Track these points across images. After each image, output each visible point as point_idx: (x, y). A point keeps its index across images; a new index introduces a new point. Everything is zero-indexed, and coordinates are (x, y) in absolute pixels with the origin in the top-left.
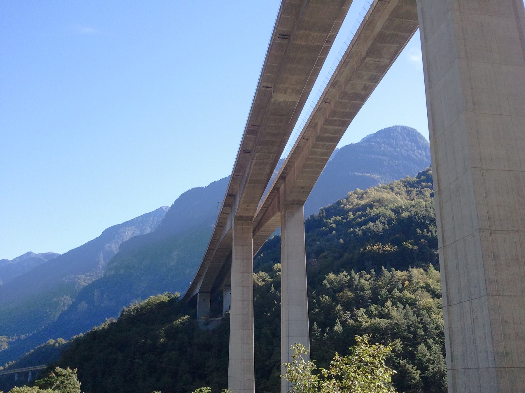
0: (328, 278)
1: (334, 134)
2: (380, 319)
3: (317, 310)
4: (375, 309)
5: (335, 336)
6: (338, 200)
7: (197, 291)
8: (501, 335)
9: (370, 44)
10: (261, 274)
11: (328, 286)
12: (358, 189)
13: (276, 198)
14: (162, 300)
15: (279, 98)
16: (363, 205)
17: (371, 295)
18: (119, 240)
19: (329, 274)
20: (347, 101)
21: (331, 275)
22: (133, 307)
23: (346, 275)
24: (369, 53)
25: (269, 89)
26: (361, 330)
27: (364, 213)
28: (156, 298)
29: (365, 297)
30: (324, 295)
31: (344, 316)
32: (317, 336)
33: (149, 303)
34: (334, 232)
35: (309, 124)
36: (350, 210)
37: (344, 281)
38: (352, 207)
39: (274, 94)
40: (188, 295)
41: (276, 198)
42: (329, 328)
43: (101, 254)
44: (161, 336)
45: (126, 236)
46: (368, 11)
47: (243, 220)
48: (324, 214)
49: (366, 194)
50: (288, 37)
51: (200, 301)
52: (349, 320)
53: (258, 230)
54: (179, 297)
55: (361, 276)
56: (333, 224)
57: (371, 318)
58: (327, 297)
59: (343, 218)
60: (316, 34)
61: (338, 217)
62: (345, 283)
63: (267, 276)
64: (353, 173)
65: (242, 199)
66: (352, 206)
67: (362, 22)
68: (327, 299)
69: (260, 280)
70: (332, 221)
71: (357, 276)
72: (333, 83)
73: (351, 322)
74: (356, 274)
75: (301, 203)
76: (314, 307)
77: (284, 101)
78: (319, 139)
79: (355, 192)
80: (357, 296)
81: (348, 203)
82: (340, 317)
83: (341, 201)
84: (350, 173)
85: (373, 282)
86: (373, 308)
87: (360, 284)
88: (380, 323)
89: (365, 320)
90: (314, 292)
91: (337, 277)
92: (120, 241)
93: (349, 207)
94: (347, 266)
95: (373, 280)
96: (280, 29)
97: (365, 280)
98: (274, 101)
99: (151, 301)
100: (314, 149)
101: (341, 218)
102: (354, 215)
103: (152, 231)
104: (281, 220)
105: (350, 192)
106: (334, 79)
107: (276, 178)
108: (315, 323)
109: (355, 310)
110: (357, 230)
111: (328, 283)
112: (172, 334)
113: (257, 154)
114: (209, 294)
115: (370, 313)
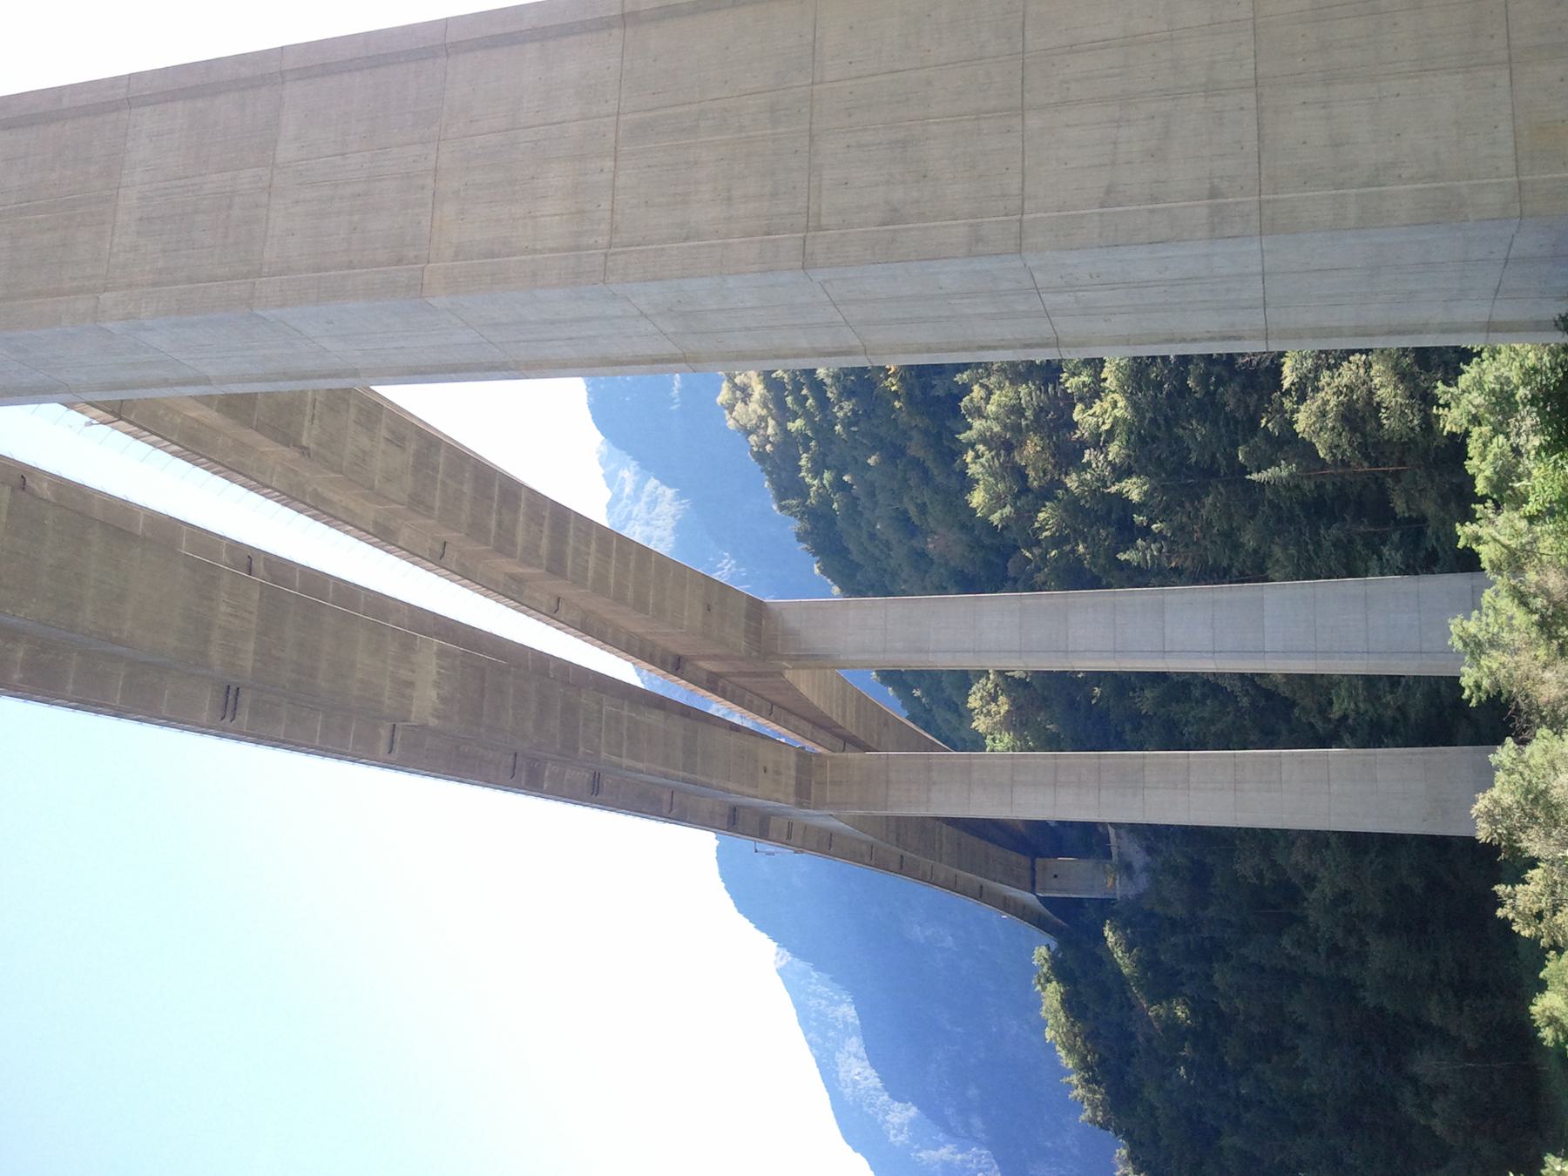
0: (985, 509)
1: (541, 525)
2: (1106, 364)
3: (1081, 548)
4: (1076, 378)
5: (1159, 498)
6: (753, 460)
7: (1028, 898)
8: (1152, 211)
9: (259, 437)
10: (974, 702)
11: (1007, 510)
12: (719, 399)
13: (742, 680)
14: (1056, 1005)
15: (426, 700)
16: (765, 388)
17: (1034, 384)
18: (879, 1103)
19: (971, 505)
20: (438, 493)
21: (974, 501)
22: (1080, 1092)
23: (973, 453)
24: (289, 439)
25: (398, 736)
26: (1140, 421)
27: (790, 388)
28: (1051, 1022)
29: (1038, 404)
30: (1037, 525)
31: (1098, 467)
32: (1160, 551)
33: (1066, 1044)
34: (846, 478)
35: (512, 599)
36: (781, 425)
37: (993, 462)
38: (773, 419)
39: (413, 720)
40: (1040, 923)
41: (742, 680)
42: (1135, 516)
43: (922, 1155)
44: (1168, 1016)
45: (866, 1079)
46: (154, 446)
47: (810, 781)
48: (794, 502)
49: (735, 377)
50: (233, 688)
51: (1059, 890)
52: (1111, 454)
53: (840, 727)
54: (1049, 949)
55: (979, 413)
56: (822, 479)
57: (1104, 392)
58: (1042, 516)
59: (807, 450)
60: (223, 608)
61: (803, 463)
62: (999, 460)
63: (980, 686)
64: (675, 399)
65: (745, 789)
66: (770, 420)
67: (189, 462)
68: (1046, 516)
69: (993, 707)
70: (815, 482)
71: (978, 424)
72: (383, 535)
73: (1114, 450)
74: (970, 427)
75: (756, 608)
76: (1071, 555)
77: (437, 685)
78: (556, 567)
79: (727, 409)
80: (1038, 425)
81: (761, 432)
82: (1102, 480)
83: (755, 449)
84: (675, 407)
85: (993, 379)
86: (1072, 383)
87: (1002, 416)
88: (1118, 364)
89: (1110, 409)
90: (1027, 554)
91: (981, 482)
92: (881, 1098)
93: (773, 428)
94: (951, 453)
95: (989, 376)
96: (205, 717)
97: (987, 400)
98: (438, 718)
99: (1061, 1039)
100: (589, 583)
101: (805, 455)
102: (795, 417)
103: (850, 1000)
104: (810, 668)
105: (726, 422)
106: (370, 533)
107: (678, 684)
108: (1122, 557)
109: (1078, 434)
110: (841, 414)
111: (999, 511)
112: (1163, 983)
113: (604, 755)
114: (1039, 861)
115: (1087, 392)
